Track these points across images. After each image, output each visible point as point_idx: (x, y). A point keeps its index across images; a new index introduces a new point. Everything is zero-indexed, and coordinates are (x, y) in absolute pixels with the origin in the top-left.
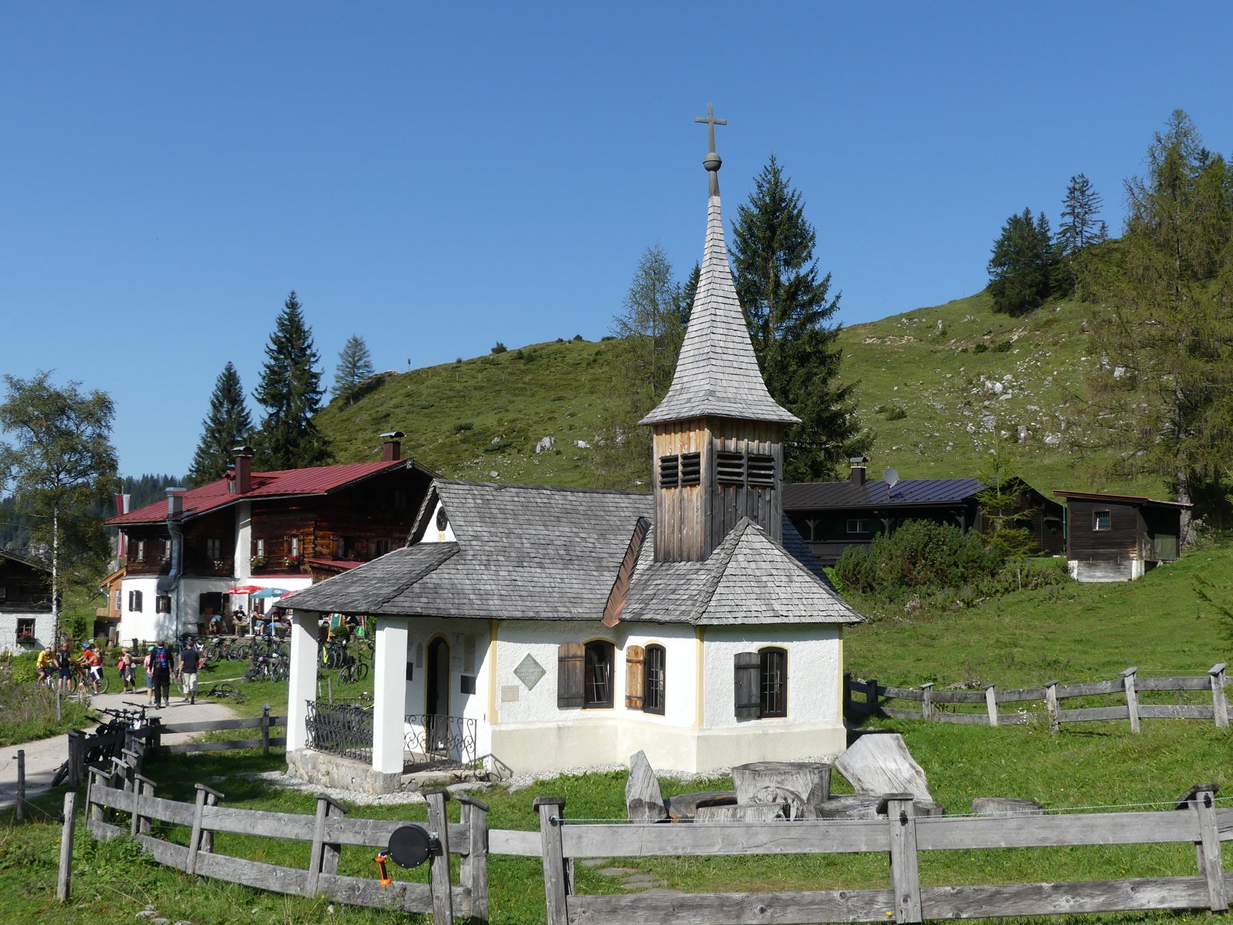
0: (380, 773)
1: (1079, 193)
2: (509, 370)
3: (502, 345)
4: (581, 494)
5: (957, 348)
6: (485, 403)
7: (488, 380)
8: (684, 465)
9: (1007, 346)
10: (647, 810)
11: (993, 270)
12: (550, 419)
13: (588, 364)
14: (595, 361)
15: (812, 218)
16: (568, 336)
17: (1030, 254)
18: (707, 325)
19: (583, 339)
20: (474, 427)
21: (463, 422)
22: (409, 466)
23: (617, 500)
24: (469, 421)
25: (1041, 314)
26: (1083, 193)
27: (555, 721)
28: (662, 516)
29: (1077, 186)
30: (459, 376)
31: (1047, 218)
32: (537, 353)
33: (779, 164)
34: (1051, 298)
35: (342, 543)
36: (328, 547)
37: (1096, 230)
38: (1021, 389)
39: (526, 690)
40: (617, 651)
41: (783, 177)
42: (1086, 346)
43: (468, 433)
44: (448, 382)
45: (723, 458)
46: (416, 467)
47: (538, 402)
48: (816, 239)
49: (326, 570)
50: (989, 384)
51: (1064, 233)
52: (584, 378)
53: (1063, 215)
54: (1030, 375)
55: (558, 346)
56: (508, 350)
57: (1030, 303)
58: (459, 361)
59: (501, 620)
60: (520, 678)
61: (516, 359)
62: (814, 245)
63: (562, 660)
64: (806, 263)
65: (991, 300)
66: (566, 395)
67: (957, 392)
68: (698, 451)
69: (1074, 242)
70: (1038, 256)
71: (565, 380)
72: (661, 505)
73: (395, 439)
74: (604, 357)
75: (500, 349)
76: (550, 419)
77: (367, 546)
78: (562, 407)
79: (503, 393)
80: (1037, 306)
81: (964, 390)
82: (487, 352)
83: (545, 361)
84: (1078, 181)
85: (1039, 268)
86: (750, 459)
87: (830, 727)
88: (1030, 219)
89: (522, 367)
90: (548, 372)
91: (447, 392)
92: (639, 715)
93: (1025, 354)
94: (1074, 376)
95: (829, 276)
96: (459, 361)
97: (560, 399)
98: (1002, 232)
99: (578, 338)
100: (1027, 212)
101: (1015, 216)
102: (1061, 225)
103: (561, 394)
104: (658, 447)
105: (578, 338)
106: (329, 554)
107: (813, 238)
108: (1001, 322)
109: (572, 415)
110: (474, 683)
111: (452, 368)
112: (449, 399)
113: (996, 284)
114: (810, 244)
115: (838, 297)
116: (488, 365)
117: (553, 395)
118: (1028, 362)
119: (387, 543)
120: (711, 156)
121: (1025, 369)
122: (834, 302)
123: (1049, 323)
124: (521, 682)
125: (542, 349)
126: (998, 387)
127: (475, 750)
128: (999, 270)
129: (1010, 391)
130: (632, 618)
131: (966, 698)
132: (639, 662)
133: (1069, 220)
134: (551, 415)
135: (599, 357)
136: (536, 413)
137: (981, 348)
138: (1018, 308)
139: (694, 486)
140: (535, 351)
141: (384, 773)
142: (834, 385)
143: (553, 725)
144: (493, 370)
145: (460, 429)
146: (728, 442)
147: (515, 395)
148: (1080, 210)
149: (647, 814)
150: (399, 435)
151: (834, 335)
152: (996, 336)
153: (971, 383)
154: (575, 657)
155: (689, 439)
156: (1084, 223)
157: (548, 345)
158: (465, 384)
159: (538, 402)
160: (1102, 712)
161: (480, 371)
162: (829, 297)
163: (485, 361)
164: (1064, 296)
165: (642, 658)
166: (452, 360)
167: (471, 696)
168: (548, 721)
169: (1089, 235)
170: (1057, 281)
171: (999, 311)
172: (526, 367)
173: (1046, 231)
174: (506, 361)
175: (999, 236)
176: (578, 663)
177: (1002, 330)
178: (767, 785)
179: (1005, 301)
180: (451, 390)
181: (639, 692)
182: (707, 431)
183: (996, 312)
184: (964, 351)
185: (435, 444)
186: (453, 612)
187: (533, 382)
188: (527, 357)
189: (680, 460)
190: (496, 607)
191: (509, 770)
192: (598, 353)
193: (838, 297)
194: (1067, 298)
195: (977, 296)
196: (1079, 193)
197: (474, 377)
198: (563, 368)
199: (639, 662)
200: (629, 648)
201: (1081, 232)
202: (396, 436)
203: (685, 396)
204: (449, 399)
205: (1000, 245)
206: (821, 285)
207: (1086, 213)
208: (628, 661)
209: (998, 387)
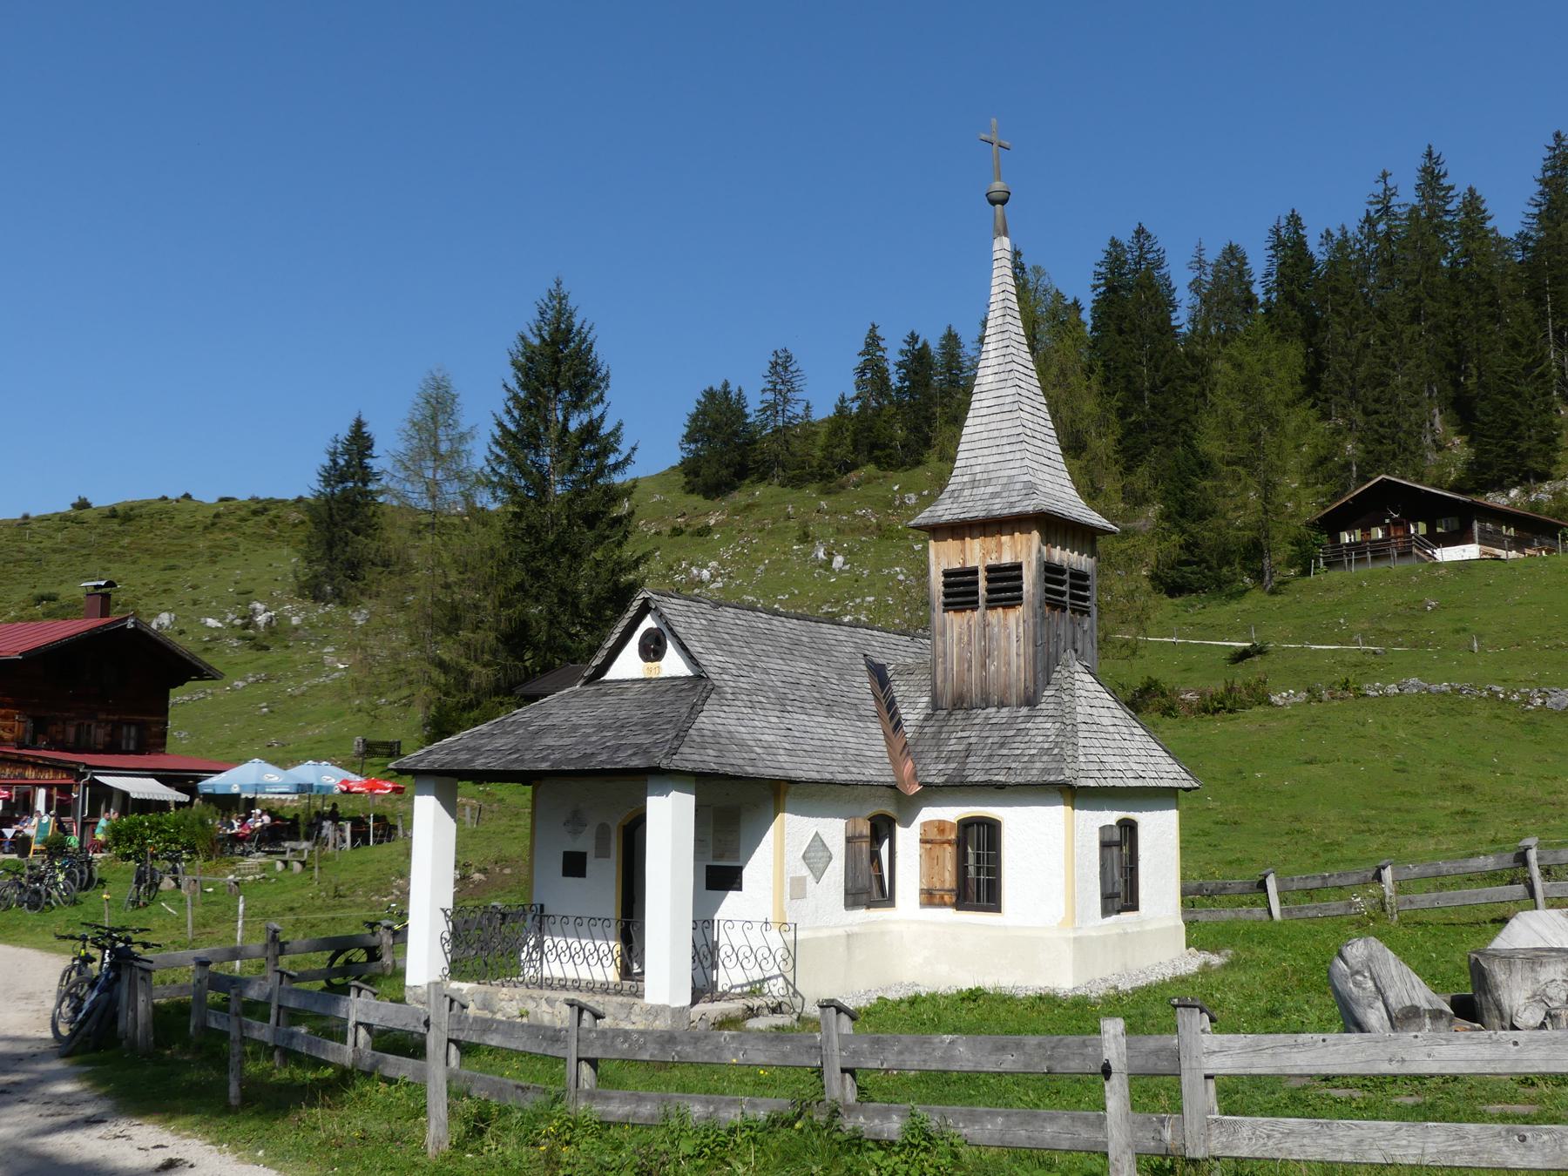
0: (664, 1008)
1: (781, 370)
2: (98, 530)
3: (85, 499)
4: (813, 624)
5: (650, 530)
6: (69, 569)
7: (71, 542)
8: (989, 580)
9: (705, 531)
10: (1427, 1021)
11: (686, 446)
12: (165, 591)
13: (206, 528)
14: (213, 524)
15: (605, 353)
16: (174, 493)
17: (729, 431)
18: (1008, 400)
19: (193, 498)
20: (60, 597)
21: (46, 591)
22: (130, 626)
23: (835, 632)
24: (53, 590)
25: (739, 497)
26: (786, 368)
27: (843, 926)
28: (945, 648)
29: (779, 361)
30: (30, 534)
31: (745, 393)
32: (136, 512)
33: (565, 288)
34: (747, 481)
35: (30, 725)
36: (11, 730)
37: (799, 410)
38: (730, 578)
39: (814, 882)
40: (900, 831)
41: (571, 303)
42: (797, 534)
43: (53, 605)
44: (14, 541)
45: (1051, 572)
46: (139, 627)
47: (142, 570)
48: (611, 380)
49: (12, 761)
50: (695, 571)
51: (764, 410)
52: (201, 544)
53: (764, 391)
54: (737, 562)
55: (162, 505)
56: (94, 506)
57: (726, 485)
58: (26, 517)
59: (792, 782)
60: (808, 864)
61: (107, 517)
62: (607, 386)
63: (849, 840)
64: (597, 407)
65: (683, 479)
66: (177, 563)
67: (657, 579)
68: (1019, 560)
69: (775, 421)
70: (736, 434)
71: (176, 545)
72: (943, 634)
73: (103, 590)
74: (225, 520)
75: (83, 505)
76: (165, 591)
77: (64, 732)
78: (178, 577)
79: (93, 558)
80: (734, 488)
81: (665, 577)
82: (65, 507)
83: (146, 522)
84: (780, 355)
85: (738, 446)
86: (1071, 574)
87: (1172, 924)
88: (729, 393)
89: (116, 528)
90: (151, 535)
91: (15, 554)
92: (948, 915)
93: (727, 540)
94: (789, 565)
95: (621, 424)
96: (26, 517)
97: (172, 568)
98: (696, 404)
99: (187, 496)
100: (726, 385)
101: (711, 389)
102: (762, 402)
103: (172, 562)
104: (937, 557)
105: (187, 496)
106: (12, 740)
107: (606, 378)
108: (696, 504)
109: (194, 587)
110: (741, 873)
111: (19, 525)
112: (18, 563)
113: (689, 462)
114: (603, 385)
115: (634, 449)
116: (68, 524)
117: (161, 563)
118: (734, 549)
119: (89, 726)
120: (998, 185)
121: (731, 556)
122: (629, 455)
123: (749, 507)
124: (809, 872)
125: (141, 507)
126: (706, 574)
127: (794, 966)
128: (693, 447)
129: (719, 579)
130: (946, 781)
131: (1225, 888)
132: (949, 842)
133: (770, 396)
134: (166, 587)
135: (217, 520)
136: (144, 584)
137: (677, 532)
138: (715, 490)
139: (1013, 606)
140: (132, 509)
141: (672, 1006)
142: (628, 552)
143: (840, 932)
144: (76, 530)
145: (40, 599)
146: (1053, 550)
147: (109, 562)
148: (782, 387)
149: (1428, 1026)
150: (110, 584)
151: (628, 492)
152: (691, 518)
153: (672, 569)
154: (861, 837)
155: (1000, 545)
156: (786, 401)
157: (149, 503)
158: (39, 545)
159: (142, 570)
160: (1477, 894)
161: (60, 530)
162: (624, 448)
163: (64, 518)
164: (762, 479)
165: (953, 836)
166: (17, 515)
167: (732, 894)
168: (836, 927)
169: (791, 415)
170: (755, 462)
171: (692, 491)
172: (121, 528)
173: (744, 407)
174: (94, 519)
175: (692, 408)
176: (864, 845)
177: (696, 512)
178: (1552, 978)
179: (700, 481)
180: (19, 551)
181: (948, 878)
182: (1035, 535)
183: (687, 493)
184: (658, 533)
185: (6, 617)
186: (750, 770)
187: (133, 546)
188: (123, 516)
189: (982, 575)
190: (785, 765)
191: (801, 996)
192: (217, 516)
193: (634, 449)
194: (766, 482)
195: (664, 474)
196: (781, 370)
197: (50, 537)
198: (172, 531)
199: (949, 842)
200: (924, 825)
201: (783, 410)
202: (106, 586)
203: (990, 489)
204: (18, 563)
205: (694, 419)
206: (610, 434)
207: (789, 390)
208: (923, 841)
209: (706, 574)
